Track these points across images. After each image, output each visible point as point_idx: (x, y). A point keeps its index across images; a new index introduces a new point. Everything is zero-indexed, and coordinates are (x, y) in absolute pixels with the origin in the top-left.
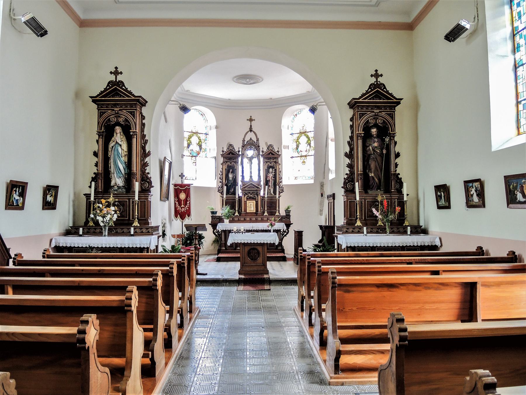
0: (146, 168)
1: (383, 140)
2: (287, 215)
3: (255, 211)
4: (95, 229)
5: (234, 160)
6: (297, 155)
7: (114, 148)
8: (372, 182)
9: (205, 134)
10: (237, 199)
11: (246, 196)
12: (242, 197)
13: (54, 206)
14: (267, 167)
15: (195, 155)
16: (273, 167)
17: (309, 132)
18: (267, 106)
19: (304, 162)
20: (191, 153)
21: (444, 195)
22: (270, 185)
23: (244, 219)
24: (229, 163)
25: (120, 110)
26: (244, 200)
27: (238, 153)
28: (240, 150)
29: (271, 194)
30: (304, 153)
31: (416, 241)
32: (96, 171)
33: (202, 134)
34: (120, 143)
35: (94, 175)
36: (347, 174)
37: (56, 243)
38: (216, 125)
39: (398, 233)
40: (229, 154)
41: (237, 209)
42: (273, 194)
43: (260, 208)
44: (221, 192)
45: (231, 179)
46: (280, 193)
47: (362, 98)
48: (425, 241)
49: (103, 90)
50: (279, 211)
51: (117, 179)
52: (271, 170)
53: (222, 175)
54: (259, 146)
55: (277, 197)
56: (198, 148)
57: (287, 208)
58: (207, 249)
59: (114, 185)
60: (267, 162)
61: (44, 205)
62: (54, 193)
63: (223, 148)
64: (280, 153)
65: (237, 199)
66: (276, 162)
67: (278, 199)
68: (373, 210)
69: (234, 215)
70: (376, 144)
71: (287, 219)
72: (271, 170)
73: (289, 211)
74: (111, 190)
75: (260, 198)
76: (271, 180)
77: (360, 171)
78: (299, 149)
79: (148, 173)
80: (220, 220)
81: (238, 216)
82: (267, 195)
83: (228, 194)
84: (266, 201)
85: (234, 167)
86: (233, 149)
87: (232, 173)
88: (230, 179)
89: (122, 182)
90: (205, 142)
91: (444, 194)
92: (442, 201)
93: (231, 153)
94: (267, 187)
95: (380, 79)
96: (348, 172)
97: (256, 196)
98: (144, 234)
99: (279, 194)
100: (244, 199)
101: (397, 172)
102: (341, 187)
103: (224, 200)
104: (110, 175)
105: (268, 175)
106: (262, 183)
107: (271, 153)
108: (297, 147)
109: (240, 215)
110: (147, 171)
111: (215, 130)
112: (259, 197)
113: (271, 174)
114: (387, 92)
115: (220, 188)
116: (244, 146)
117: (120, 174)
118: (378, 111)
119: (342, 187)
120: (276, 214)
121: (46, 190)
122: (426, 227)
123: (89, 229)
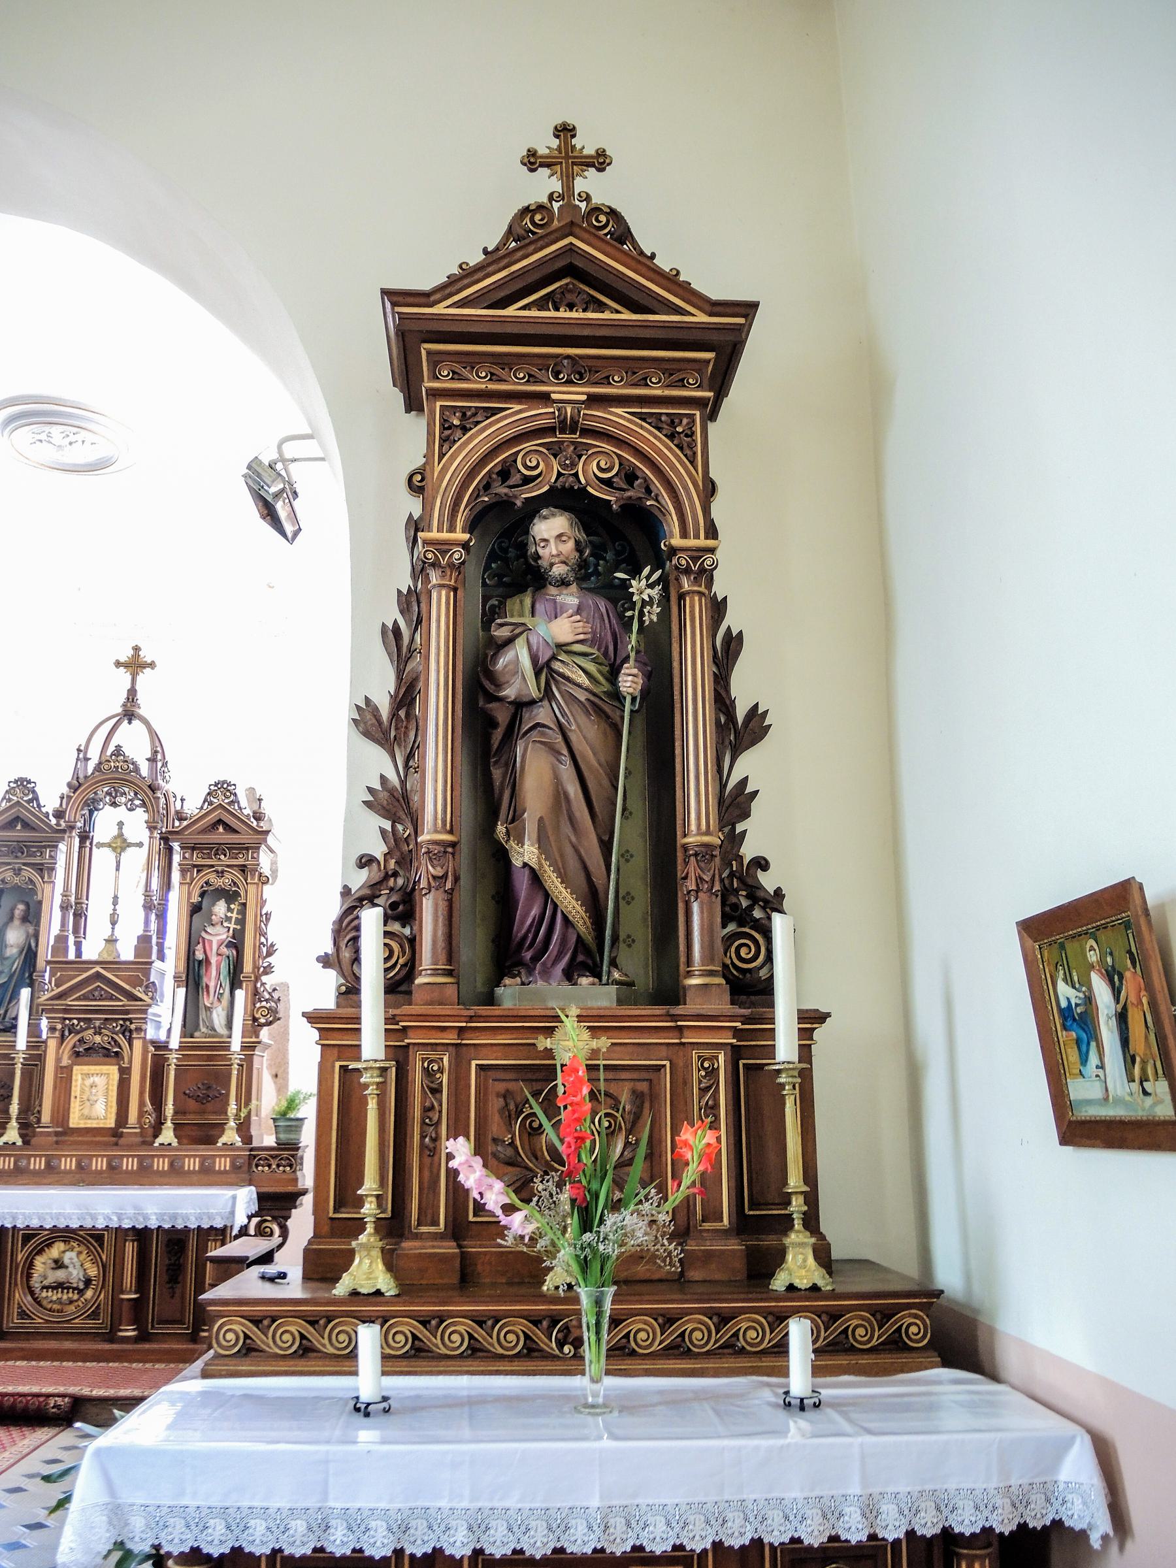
1: (619, 595)
3: (111, 1123)
5: (33, 855)
8: (535, 912)
10: (20, 1059)
11: (71, 1040)
16: (230, 896)
21: (1117, 997)
24: (10, 873)
25: (594, 400)
26: (58, 1059)
31: (855, 1489)
36: (365, 861)
37: (116, 1512)
39: (779, 1309)
40: (10, 824)
43: (142, 1104)
46: (262, 1025)
47: (456, 298)
48: (952, 1486)
52: (220, 908)
60: (200, 868)
64: (264, 826)
65: (20, 1059)
66: (244, 866)
67: (236, 1060)
68: (450, 1157)
70: (563, 629)
71: (278, 1166)
73: (298, 1119)
75: (145, 1051)
76: (214, 960)
77: (435, 824)
85: (33, 892)
86: (29, 802)
87: (25, 919)
91: (1116, 993)
92: (1101, 1066)
95: (588, 183)
96: (378, 849)
97: (121, 1039)
101: (748, 851)
102: (319, 959)
107: (220, 821)
109: (26, 1142)
114: (644, 262)
116: (80, 785)
118: (578, 393)
119: (326, 961)
122: (977, 1288)
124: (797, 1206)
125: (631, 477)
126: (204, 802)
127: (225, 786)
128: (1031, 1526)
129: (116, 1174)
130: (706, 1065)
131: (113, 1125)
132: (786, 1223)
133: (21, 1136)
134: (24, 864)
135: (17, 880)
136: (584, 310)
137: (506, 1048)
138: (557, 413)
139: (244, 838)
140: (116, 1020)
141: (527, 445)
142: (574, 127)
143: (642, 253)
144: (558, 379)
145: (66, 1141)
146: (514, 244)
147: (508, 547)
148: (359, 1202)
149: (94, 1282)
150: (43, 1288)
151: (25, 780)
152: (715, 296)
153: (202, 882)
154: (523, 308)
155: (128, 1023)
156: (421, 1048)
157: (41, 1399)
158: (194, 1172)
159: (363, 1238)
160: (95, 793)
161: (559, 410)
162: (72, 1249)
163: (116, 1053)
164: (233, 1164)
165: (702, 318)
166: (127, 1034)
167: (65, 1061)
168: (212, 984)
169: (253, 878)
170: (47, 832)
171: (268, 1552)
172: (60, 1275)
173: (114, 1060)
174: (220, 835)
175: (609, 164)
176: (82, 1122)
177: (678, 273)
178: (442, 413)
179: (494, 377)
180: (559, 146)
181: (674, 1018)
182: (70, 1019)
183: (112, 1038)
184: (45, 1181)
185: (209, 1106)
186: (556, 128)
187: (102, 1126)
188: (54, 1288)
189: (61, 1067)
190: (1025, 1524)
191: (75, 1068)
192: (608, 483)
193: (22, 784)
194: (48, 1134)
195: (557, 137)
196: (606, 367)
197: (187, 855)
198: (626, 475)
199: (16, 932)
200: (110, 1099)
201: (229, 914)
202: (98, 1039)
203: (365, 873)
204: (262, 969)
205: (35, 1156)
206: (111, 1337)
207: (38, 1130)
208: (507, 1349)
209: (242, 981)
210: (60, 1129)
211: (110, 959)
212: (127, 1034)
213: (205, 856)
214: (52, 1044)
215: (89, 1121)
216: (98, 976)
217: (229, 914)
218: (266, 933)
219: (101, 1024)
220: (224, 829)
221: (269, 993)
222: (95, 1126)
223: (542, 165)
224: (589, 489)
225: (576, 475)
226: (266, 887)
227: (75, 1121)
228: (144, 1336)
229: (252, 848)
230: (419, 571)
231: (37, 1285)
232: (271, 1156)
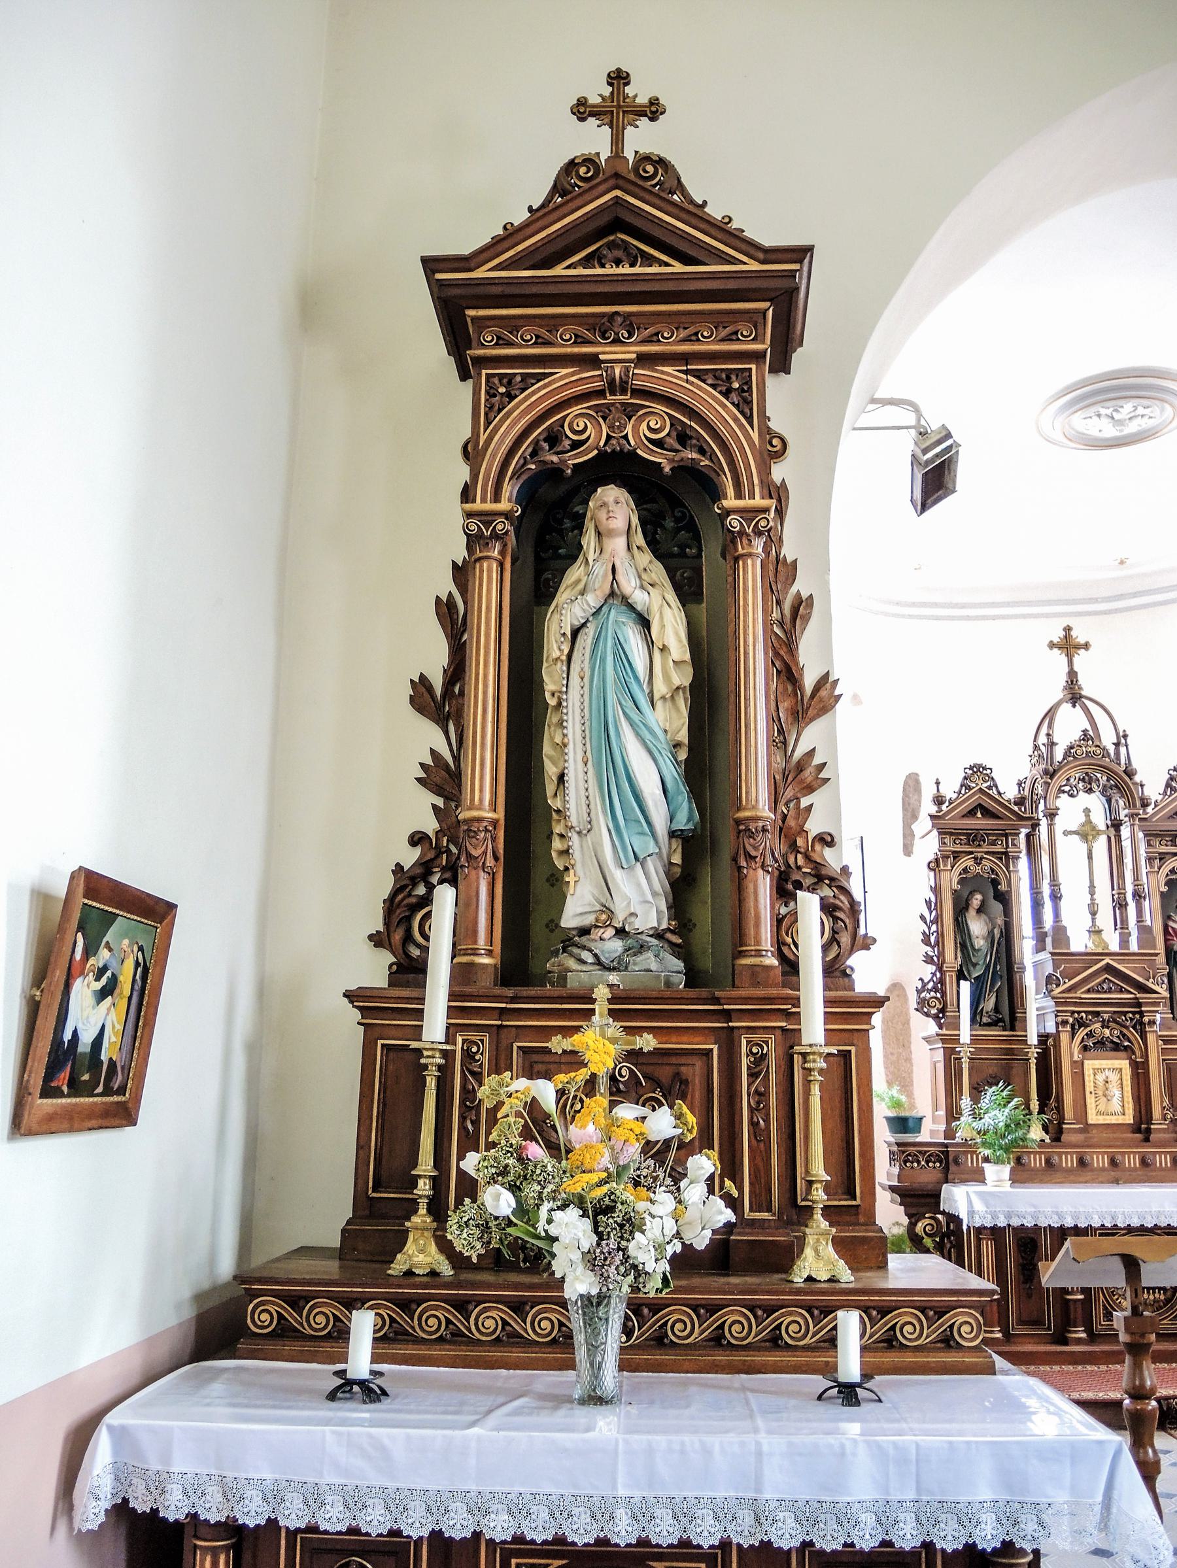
0: (805, 802)
3: (1129, 1119)
4: (462, 1306)
7: (586, 639)
11: (1081, 1033)
13: (122, 1090)
18: (1094, 600)
24: (971, 863)
25: (643, 360)
32: (431, 826)
34: (639, 598)
35: (417, 852)
36: (417, 839)
37: (121, 1475)
40: (971, 813)
44: (934, 1011)
45: (980, 943)
49: (520, 217)
51: (618, 876)
53: (938, 920)
54: (1130, 773)
59: (589, 920)
61: (36, 1081)
62: (137, 964)
63: (938, 783)
74: (572, 964)
79: (827, 840)
86: (990, 788)
87: (979, 911)
89: (650, 898)
96: (431, 826)
98: (910, 1358)
100: (1069, 1049)
103: (965, 1053)
104: (557, 844)
109: (1057, 1138)
110: (814, 826)
114: (695, 213)
115: (929, 991)
116: (1055, 771)
117: (643, 834)
119: (377, 940)
121: (61, 928)
123: (406, 1305)
124: (424, 1188)
125: (684, 438)
126: (962, 786)
128: (980, 1547)
129: (1152, 1171)
130: (755, 1050)
132: (411, 1208)
134: (987, 853)
136: (632, 265)
137: (833, 1033)
138: (604, 374)
140: (1125, 1013)
141: (576, 410)
142: (628, 74)
143: (692, 202)
144: (604, 338)
146: (560, 199)
147: (563, 518)
148: (413, 1182)
151: (980, 766)
152: (767, 241)
154: (568, 267)
155: (1137, 1016)
156: (460, 1028)
159: (416, 1219)
161: (606, 372)
163: (1126, 1047)
165: (754, 266)
166: (1138, 1027)
169: (945, 865)
170: (1011, 819)
171: (798, 1544)
175: (662, 113)
177: (730, 219)
178: (487, 381)
179: (540, 342)
180: (612, 93)
181: (716, 1001)
182: (1079, 1013)
183: (1121, 1032)
184: (1081, 1179)
186: (609, 75)
187: (1120, 1122)
190: (974, 1545)
191: (1086, 1062)
192: (659, 443)
195: (610, 84)
196: (696, 323)
198: (678, 435)
203: (417, 852)
208: (316, 1330)
211: (1100, 950)
212: (1138, 1027)
214: (1065, 1038)
215: (1108, 1117)
216: (1108, 968)
223: (592, 114)
224: (639, 452)
225: (626, 437)
229: (1011, 834)
230: (474, 541)
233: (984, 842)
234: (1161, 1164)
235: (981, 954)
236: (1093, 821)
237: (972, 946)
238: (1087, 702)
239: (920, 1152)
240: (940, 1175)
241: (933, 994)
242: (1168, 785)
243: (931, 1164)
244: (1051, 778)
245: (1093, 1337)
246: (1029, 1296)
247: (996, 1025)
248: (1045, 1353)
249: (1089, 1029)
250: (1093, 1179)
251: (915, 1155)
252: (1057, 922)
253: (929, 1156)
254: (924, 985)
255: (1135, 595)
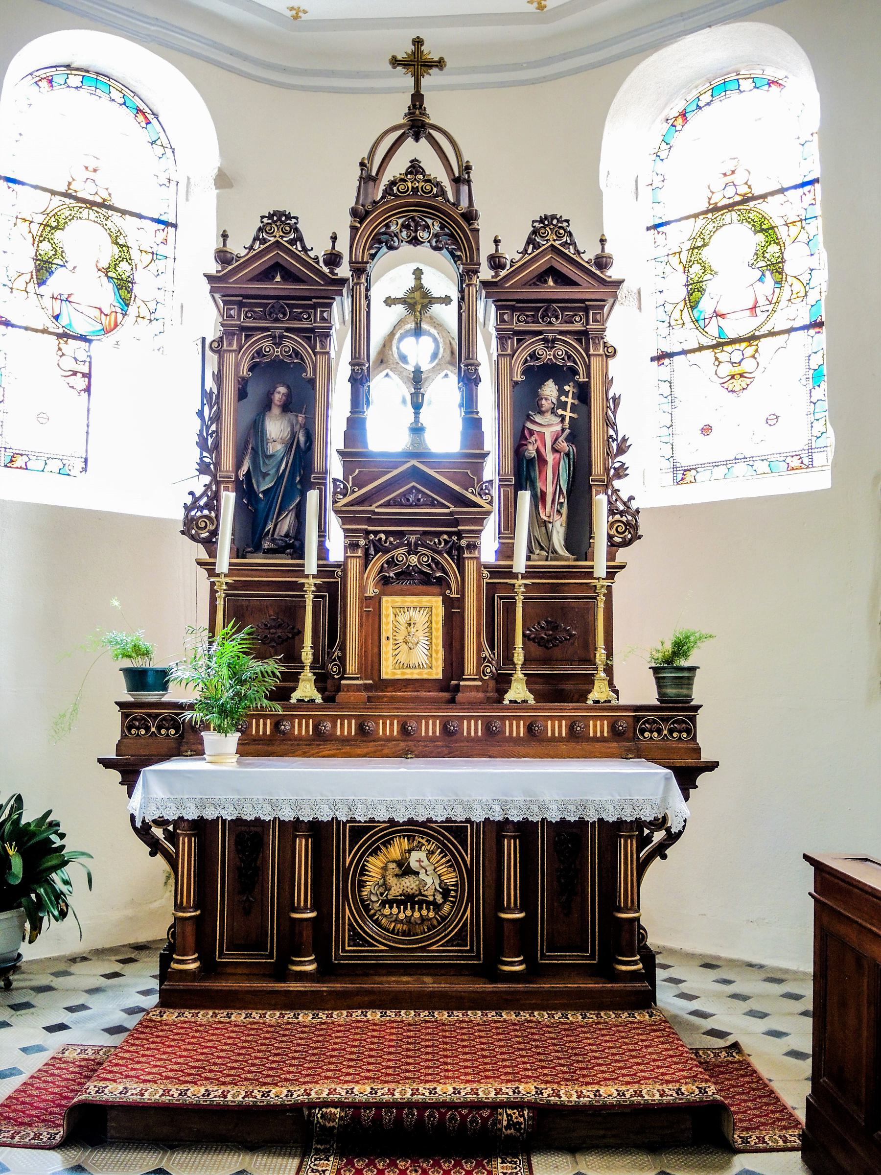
2: (666, 703)
3: (437, 673)
6: (690, 337)
9: (153, 220)
10: (310, 584)
11: (379, 561)
12: (345, 571)
14: (527, 371)
15: (81, 327)
17: (773, 193)
19: (741, 375)
20: (56, 317)
22: (544, 494)
23: (361, 728)
26: (363, 588)
27: (326, 270)
28: (343, 246)
29: (555, 551)
30: (735, 327)
33: (140, 216)
38: (219, 165)
40: (266, 275)
41: (307, 655)
42: (567, 554)
43: (480, 649)
44: (205, 535)
45: (276, 448)
50: (609, 670)
52: (550, 390)
53: (217, 418)
54: (470, 217)
55: (600, 570)
56: (107, 296)
57: (669, 647)
58: (129, 912)
60: (521, 336)
64: (613, 273)
65: (310, 584)
69: (281, 694)
71: (671, 731)
72: (550, 390)
75: (480, 577)
76: (550, 457)
78: (706, 306)
80: (182, 736)
81: (319, 707)
82: (528, 559)
83: (257, 548)
84: (520, 599)
85: (301, 367)
86: (292, 242)
87: (286, 408)
88: (270, 451)
90: (109, 198)
93: (276, 267)
94: (525, 497)
97: (447, 562)
99: (611, 557)
105: (529, 425)
106: (490, 471)
108: (690, 294)
109: (329, 699)
111: (214, 192)
112: (470, 567)
113: (549, 418)
115: (201, 509)
120: (594, 695)
126: (255, 240)
127: (555, 222)
129: (456, 742)
131: (440, 676)
133: (320, 690)
134: (288, 330)
135: (277, 352)
139: (586, 291)
140: (439, 534)
145: (379, 698)
149: (453, 893)
150: (383, 904)
151: (283, 214)
153: (525, 355)
155: (455, 538)
157: (486, 1113)
158: (561, 739)
160: (387, 226)
162: (419, 847)
164: (613, 728)
166: (455, 552)
167: (371, 591)
168: (550, 490)
169: (230, 344)
170: (319, 284)
172: (409, 884)
173: (436, 590)
174: (551, 289)
176: (399, 671)
182: (376, 533)
183: (433, 559)
184: (359, 751)
185: (557, 653)
187: (425, 676)
188: (399, 903)
189: (367, 598)
193: (279, 219)
194: (358, 688)
197: (506, 317)
199: (278, 423)
200: (434, 640)
201: (563, 398)
202: (414, 560)
204: (612, 472)
205: (342, 718)
206: (490, 972)
207: (343, 682)
209: (590, 486)
210: (371, 682)
212: (455, 552)
213: (529, 319)
214: (354, 567)
215: (408, 671)
217: (563, 398)
218: (615, 424)
219: (417, 539)
220: (555, 282)
221: (625, 503)
222: (415, 676)
226: (611, 362)
227: (388, 671)
228: (534, 971)
231: (374, 898)
232: (662, 719)
233: (285, 315)
234: (511, 731)
235: (273, 463)
236: (425, 285)
237: (264, 452)
238: (433, 132)
239: (149, 715)
240: (173, 745)
241: (206, 512)
242: (530, 241)
243: (163, 731)
244: (361, 223)
245: (326, 971)
246: (247, 912)
247: (283, 552)
248: (248, 992)
249: (389, 555)
250: (305, 753)
251: (143, 718)
252: (356, 412)
253: (162, 720)
254: (196, 500)
255: (564, 57)
